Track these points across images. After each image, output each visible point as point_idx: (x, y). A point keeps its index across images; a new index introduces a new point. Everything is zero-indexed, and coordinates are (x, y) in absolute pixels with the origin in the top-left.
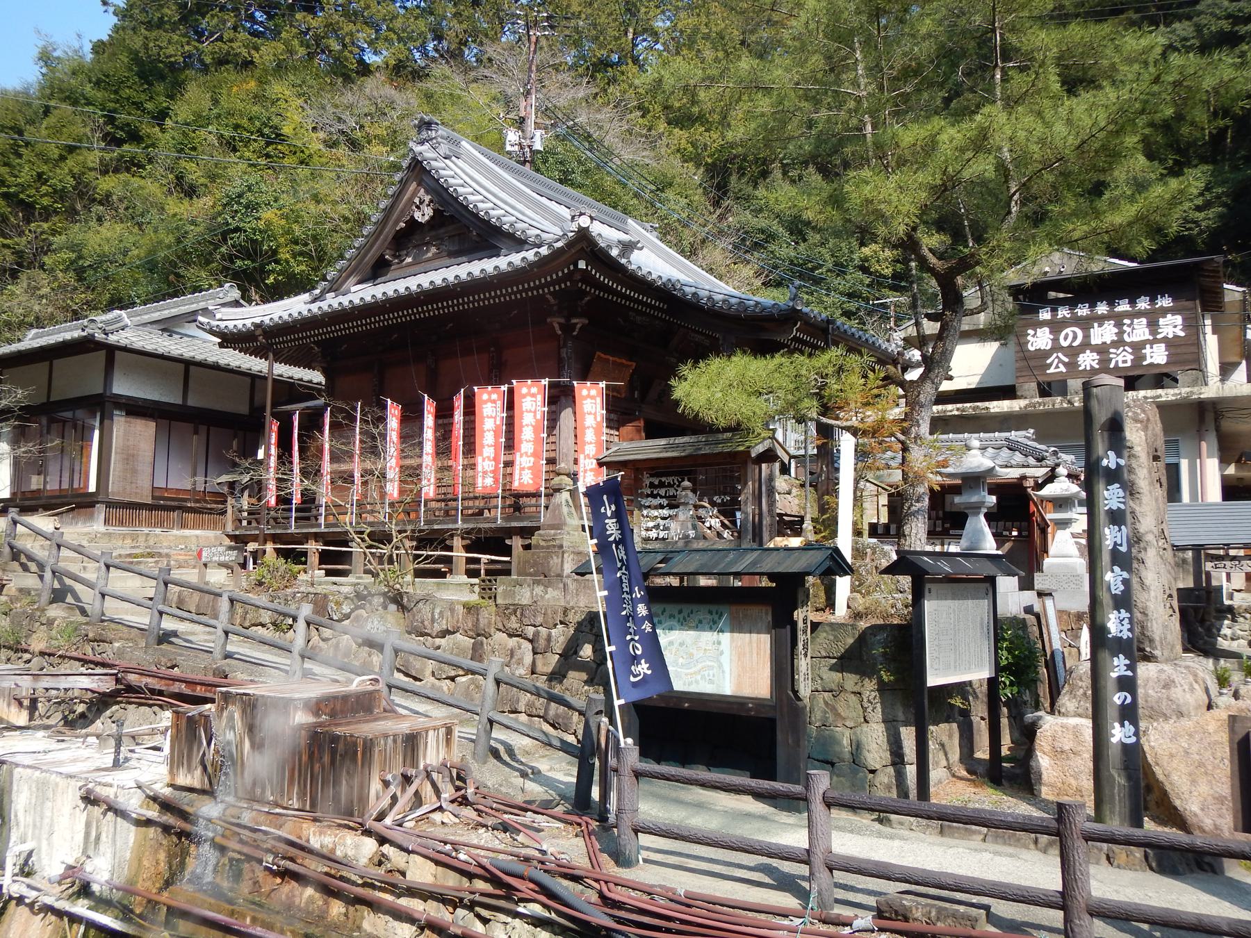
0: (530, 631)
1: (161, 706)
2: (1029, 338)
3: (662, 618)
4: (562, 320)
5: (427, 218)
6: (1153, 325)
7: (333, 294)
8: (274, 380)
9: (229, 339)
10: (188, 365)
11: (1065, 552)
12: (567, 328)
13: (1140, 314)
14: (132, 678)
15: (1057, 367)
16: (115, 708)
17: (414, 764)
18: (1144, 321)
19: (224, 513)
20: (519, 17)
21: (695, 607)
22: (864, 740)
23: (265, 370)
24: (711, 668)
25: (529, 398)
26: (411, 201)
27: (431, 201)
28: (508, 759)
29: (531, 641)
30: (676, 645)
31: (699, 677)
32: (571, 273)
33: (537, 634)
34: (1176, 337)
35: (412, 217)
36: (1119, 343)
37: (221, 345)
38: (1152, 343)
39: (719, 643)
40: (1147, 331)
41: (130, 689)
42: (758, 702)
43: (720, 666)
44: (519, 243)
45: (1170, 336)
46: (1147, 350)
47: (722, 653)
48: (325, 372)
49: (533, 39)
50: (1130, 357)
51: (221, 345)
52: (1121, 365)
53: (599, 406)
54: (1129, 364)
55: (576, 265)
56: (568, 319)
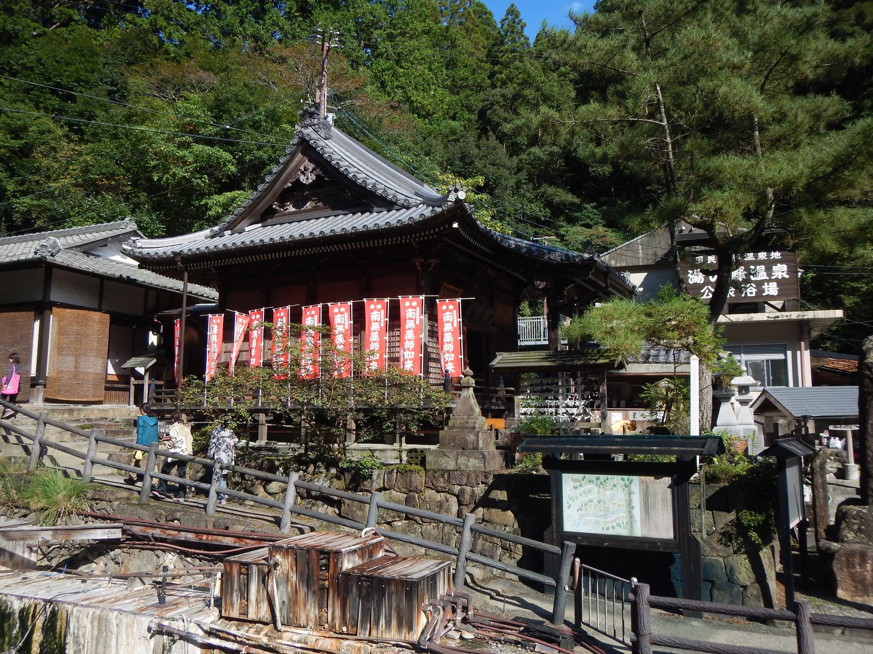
0: (456, 489)
1: (163, 551)
2: (689, 275)
3: (582, 482)
4: (422, 260)
5: (310, 181)
6: (769, 271)
7: (229, 232)
8: (188, 296)
9: (146, 262)
10: (103, 280)
11: (747, 422)
13: (761, 263)
14: (136, 530)
15: (708, 295)
16: (117, 551)
17: (435, 597)
18: (763, 267)
19: (128, 390)
20: (318, 33)
22: (735, 565)
23: (182, 288)
25: (375, 312)
26: (297, 168)
27: (314, 169)
28: (471, 585)
31: (615, 524)
33: (462, 492)
34: (783, 278)
35: (298, 180)
36: (747, 281)
37: (140, 267)
38: (769, 281)
40: (765, 274)
41: (135, 537)
42: (665, 542)
44: (389, 204)
45: (780, 277)
46: (765, 286)
48: (219, 290)
49: (326, 48)
50: (754, 290)
51: (140, 267)
52: (749, 295)
53: (316, 320)
54: (754, 295)
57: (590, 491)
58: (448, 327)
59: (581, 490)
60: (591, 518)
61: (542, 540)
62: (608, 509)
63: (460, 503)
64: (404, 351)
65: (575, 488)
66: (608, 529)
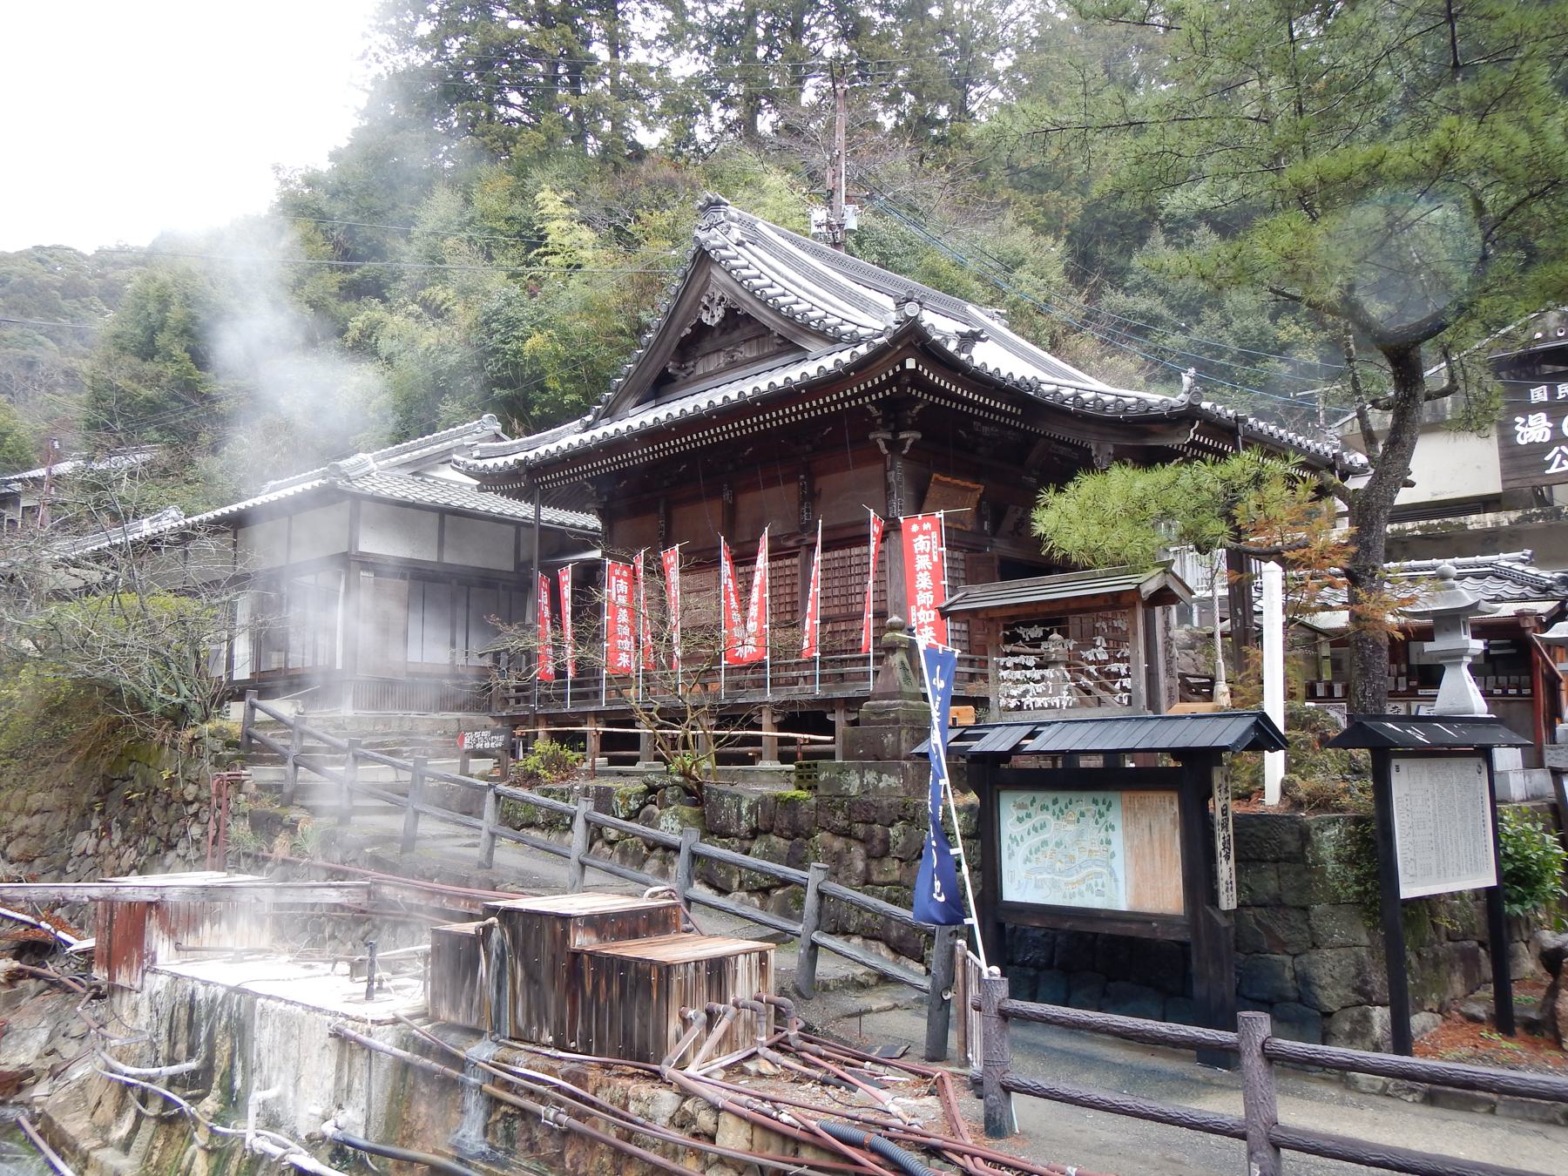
2: (1517, 428)
3: (1031, 810)
4: (889, 436)
5: (717, 320)
12: (895, 445)
21: (1074, 795)
24: (1100, 875)
29: (862, 841)
30: (1051, 845)
31: (1083, 888)
32: (897, 375)
35: (700, 320)
37: (480, 489)
39: (1109, 842)
43: (1112, 873)
47: (1113, 855)
48: (602, 515)
51: (480, 489)
55: (903, 365)
56: (895, 433)
57: (1043, 826)
58: (922, 562)
59: (1028, 824)
60: (1045, 876)
61: (1410, 1054)
62: (1072, 859)
63: (870, 856)
64: (918, 610)
65: (1020, 820)
66: (1072, 896)
